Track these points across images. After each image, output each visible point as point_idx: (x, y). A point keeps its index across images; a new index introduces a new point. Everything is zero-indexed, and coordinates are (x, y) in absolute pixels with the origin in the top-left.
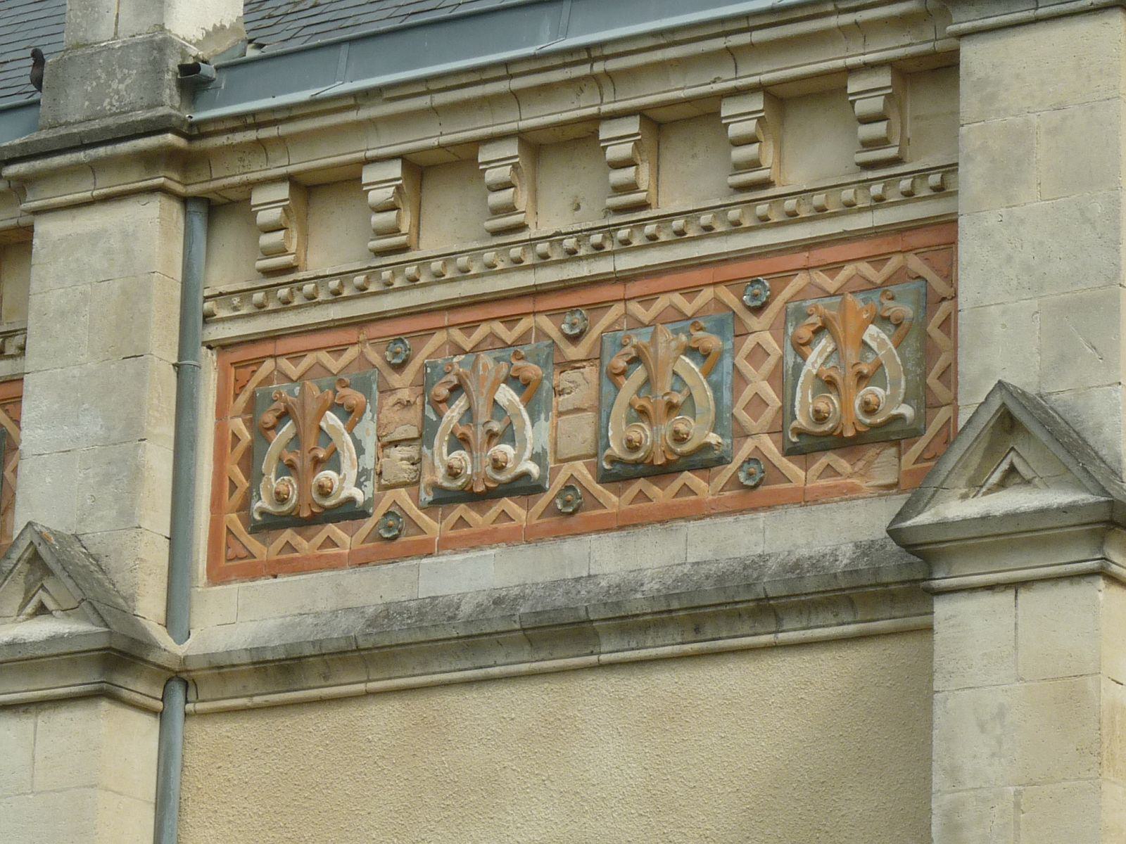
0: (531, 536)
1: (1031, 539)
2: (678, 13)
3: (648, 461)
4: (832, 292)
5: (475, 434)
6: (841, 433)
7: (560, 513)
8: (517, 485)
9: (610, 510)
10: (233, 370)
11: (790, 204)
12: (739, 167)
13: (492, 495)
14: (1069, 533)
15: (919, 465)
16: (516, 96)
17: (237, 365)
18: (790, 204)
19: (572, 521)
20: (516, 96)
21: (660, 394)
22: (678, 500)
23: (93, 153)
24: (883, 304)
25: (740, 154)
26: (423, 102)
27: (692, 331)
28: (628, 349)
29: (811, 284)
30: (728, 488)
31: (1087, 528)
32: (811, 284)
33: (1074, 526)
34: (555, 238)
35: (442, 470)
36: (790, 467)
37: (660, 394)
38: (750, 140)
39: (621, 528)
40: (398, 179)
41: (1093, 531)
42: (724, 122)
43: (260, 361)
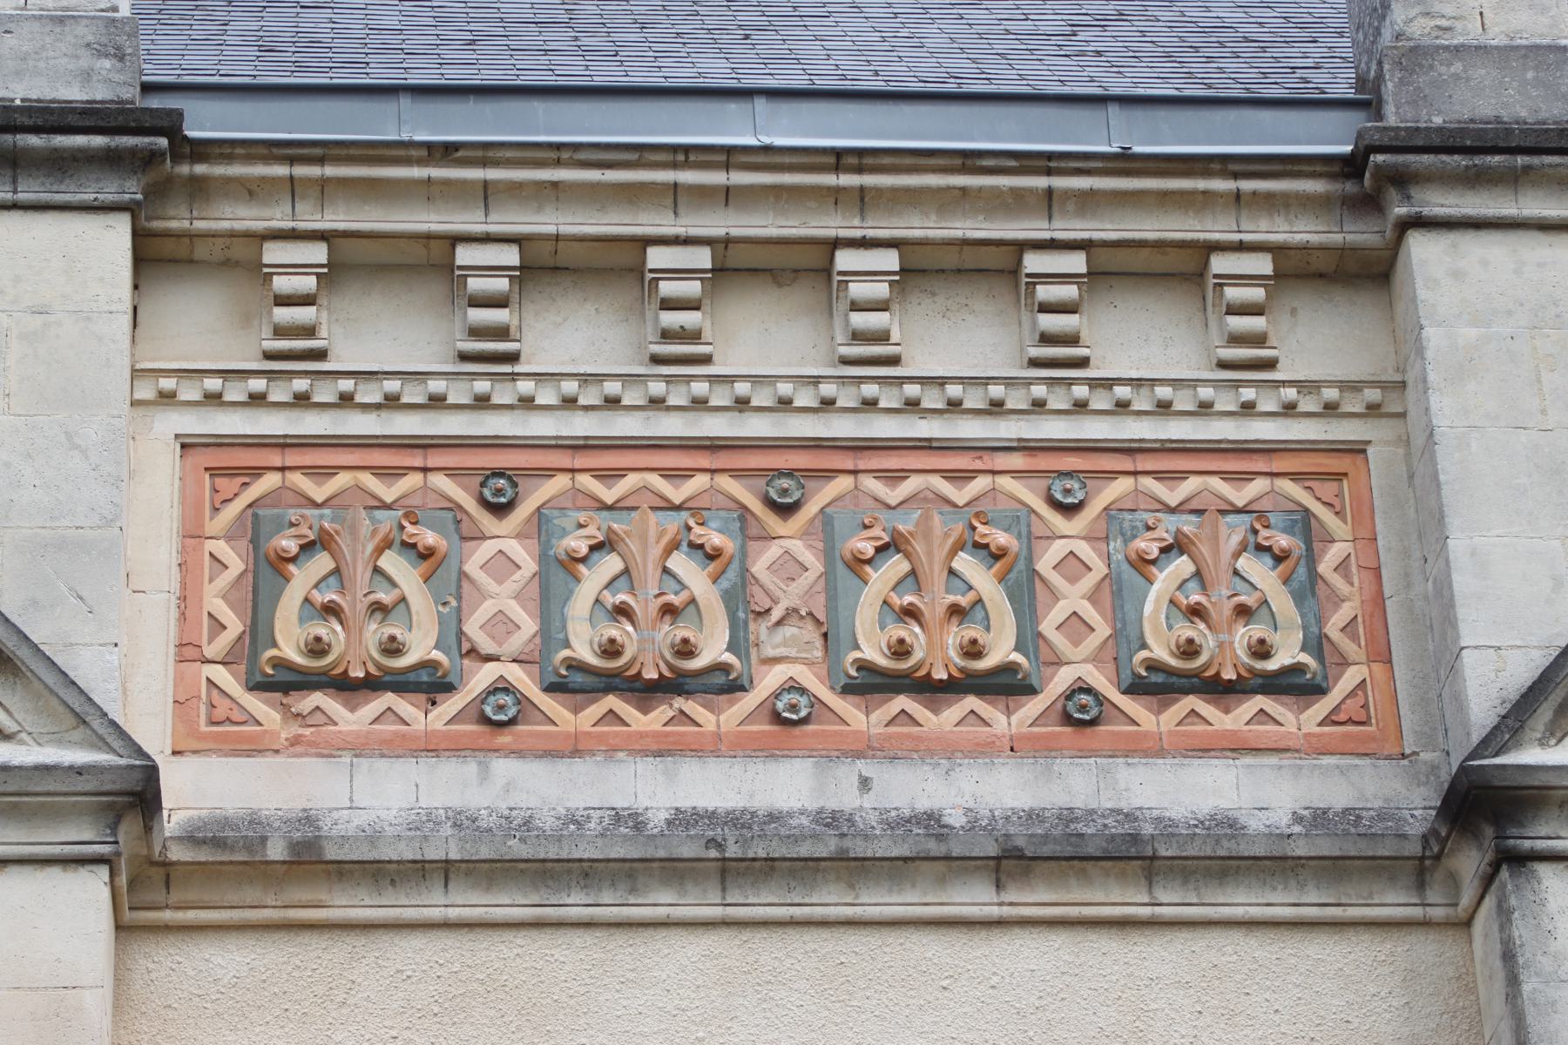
0: (431, 747)
1: (15, 805)
2: (973, 140)
3: (922, 673)
4: (677, 502)
5: (353, 605)
6: (929, 674)
7: (485, 720)
8: (412, 677)
9: (634, 728)
10: (207, 476)
11: (526, 387)
12: (1236, 339)
13: (372, 685)
14: (74, 804)
15: (1326, 729)
16: (728, 195)
17: (214, 472)
18: (912, 390)
19: (505, 739)
20: (728, 195)
21: (360, 594)
22: (596, 729)
23: (61, 140)
24: (974, 529)
25: (1049, 322)
26: (717, 178)
27: (406, 524)
28: (877, 532)
29: (713, 489)
30: (1042, 721)
31: (104, 799)
32: (577, 491)
33: (85, 794)
34: (1307, 386)
35: (953, 654)
36: (844, 706)
37: (360, 594)
38: (307, 300)
39: (659, 754)
40: (894, 273)
41: (111, 805)
42: (266, 270)
43: (257, 472)
